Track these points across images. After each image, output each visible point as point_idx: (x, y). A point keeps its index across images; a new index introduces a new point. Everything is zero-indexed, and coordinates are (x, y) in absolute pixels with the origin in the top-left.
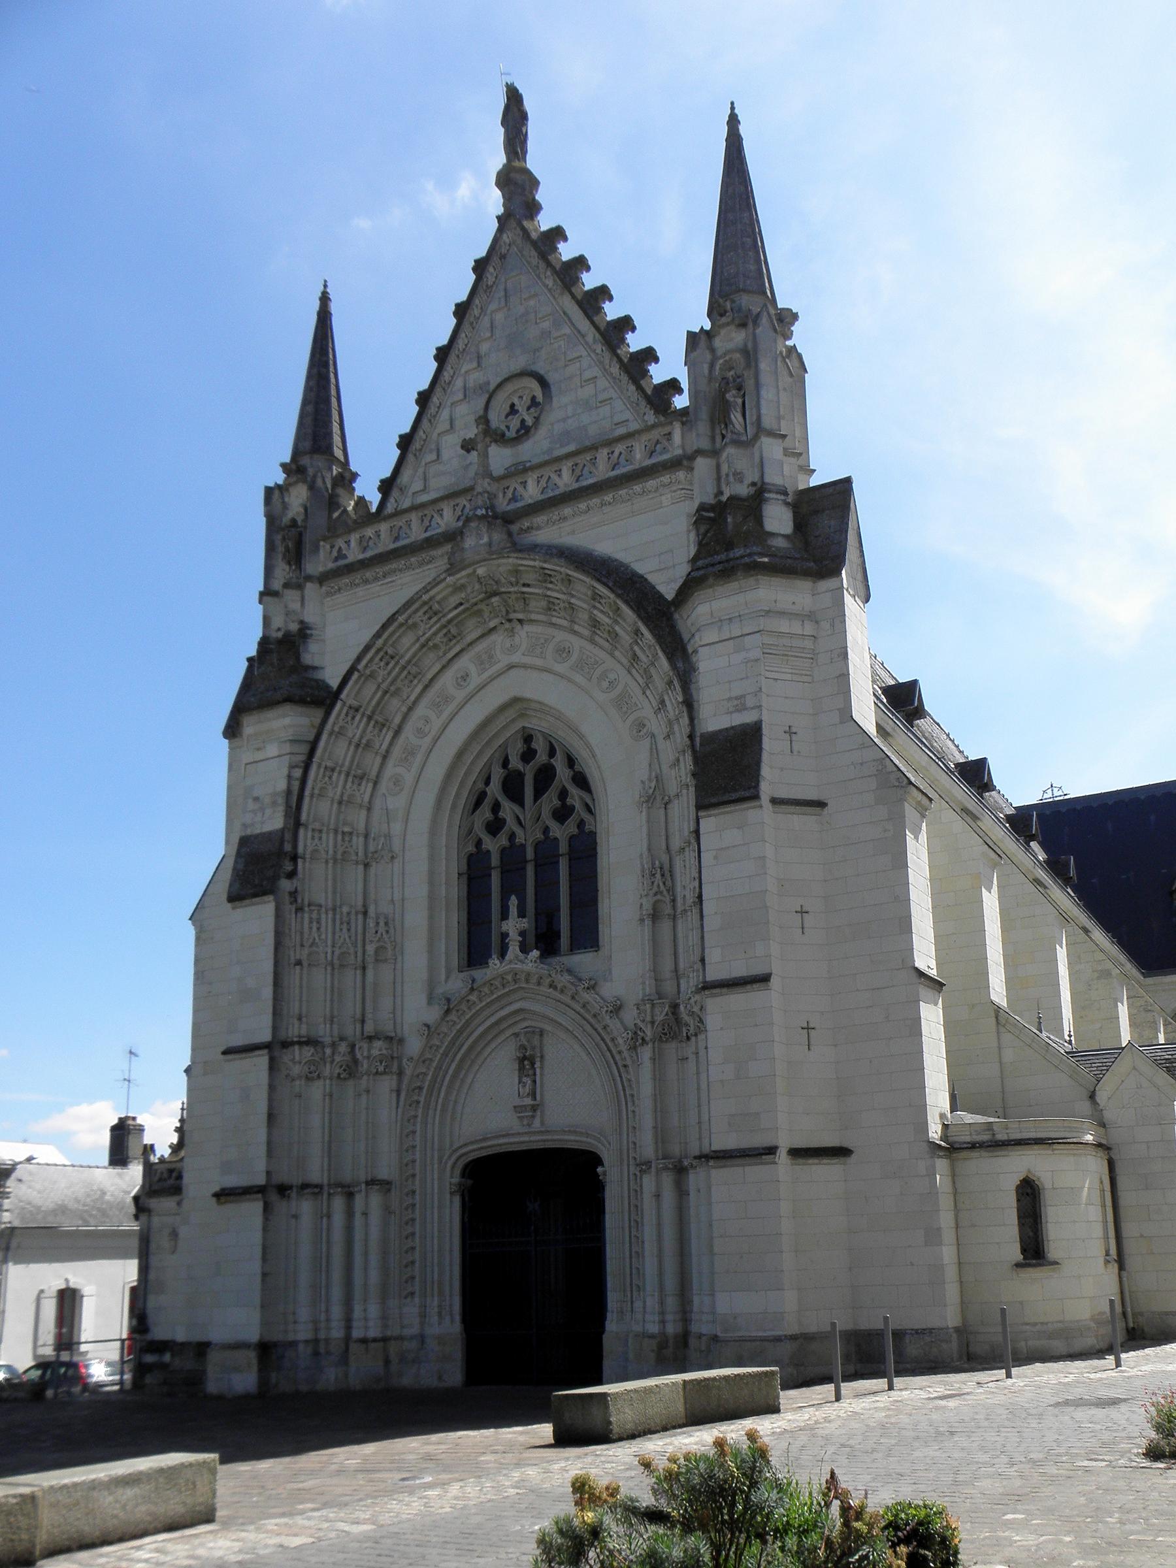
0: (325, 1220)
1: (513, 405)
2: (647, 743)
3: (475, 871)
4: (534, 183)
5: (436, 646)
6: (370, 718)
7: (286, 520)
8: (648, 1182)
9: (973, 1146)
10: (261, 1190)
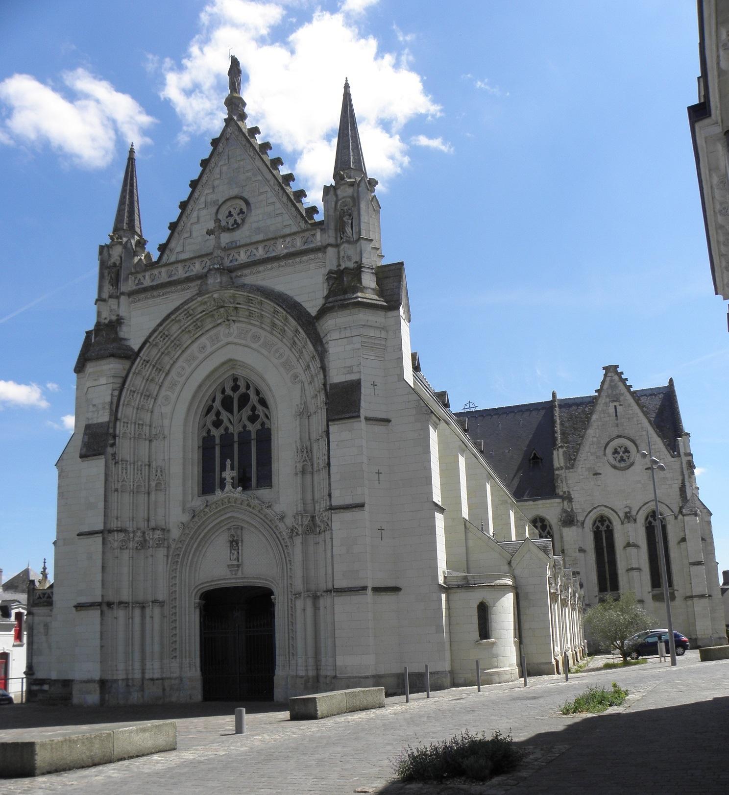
1: (230, 212)
2: (299, 386)
3: (207, 446)
4: (244, 104)
5: (189, 331)
6: (154, 366)
7: (110, 263)
8: (299, 604)
9: (458, 587)
10: (99, 604)
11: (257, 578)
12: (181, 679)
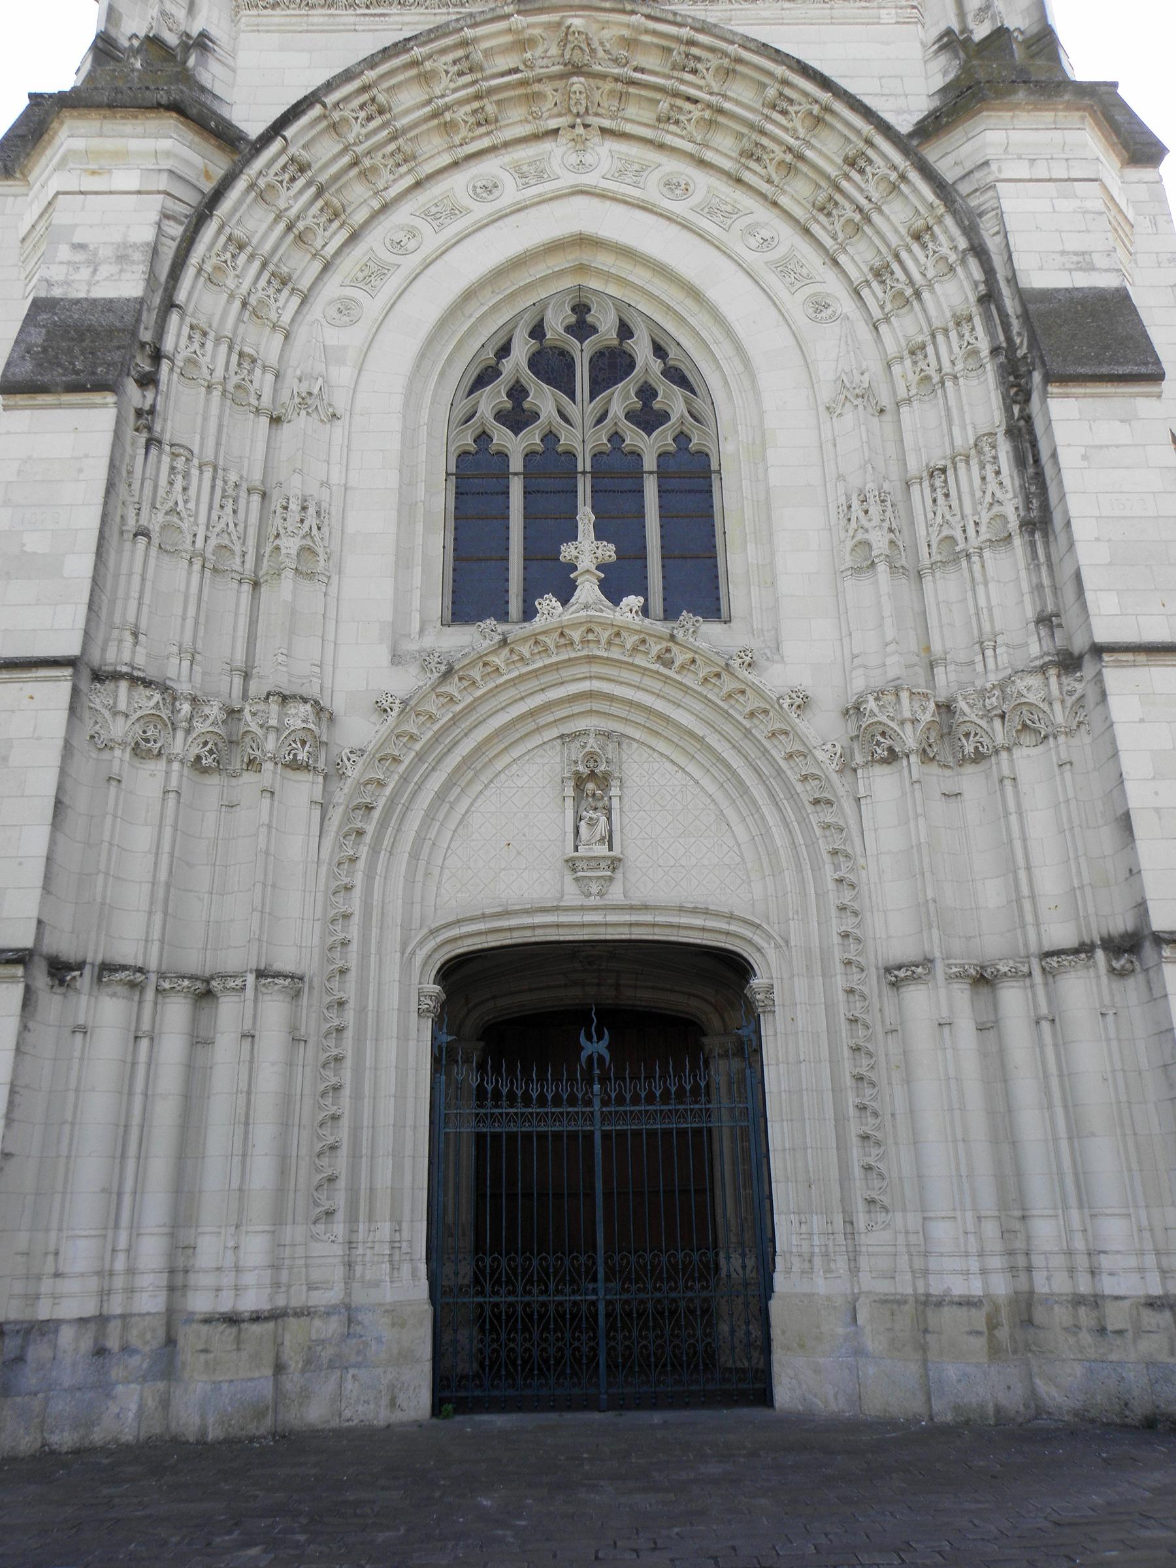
0: (144, 1043)
3: (475, 481)
11: (694, 911)
12: (349, 1313)
